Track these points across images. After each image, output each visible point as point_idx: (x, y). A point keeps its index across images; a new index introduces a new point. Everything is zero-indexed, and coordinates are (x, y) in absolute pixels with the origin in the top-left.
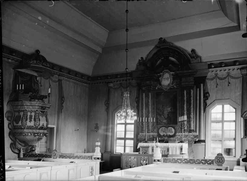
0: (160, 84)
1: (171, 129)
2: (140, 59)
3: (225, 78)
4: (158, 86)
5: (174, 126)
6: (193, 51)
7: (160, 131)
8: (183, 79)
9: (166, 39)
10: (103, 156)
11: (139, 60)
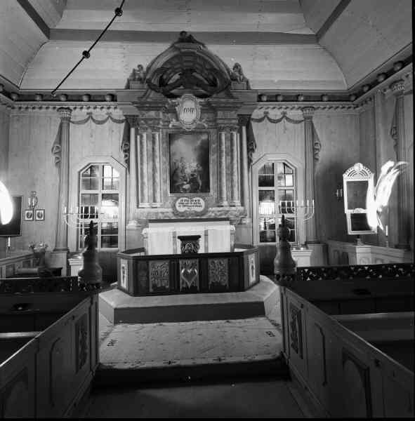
0: (177, 120)
1: (199, 201)
2: (137, 69)
3: (279, 121)
4: (174, 122)
5: (203, 194)
6: (237, 66)
7: (177, 204)
8: (220, 114)
9: (193, 35)
10: (100, 355)
11: (134, 70)
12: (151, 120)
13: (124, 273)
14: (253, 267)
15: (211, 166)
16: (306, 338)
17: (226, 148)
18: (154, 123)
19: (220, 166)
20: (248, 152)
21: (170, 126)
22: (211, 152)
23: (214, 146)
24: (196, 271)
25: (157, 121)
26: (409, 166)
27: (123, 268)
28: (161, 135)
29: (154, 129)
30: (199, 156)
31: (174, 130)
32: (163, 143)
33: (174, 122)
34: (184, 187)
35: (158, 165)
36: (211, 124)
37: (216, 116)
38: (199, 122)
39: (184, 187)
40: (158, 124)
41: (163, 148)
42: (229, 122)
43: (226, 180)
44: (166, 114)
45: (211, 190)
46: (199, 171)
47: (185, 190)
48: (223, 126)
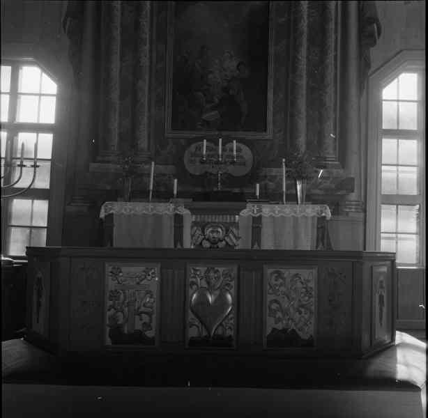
5: (250, 136)
13: (39, 296)
14: (381, 297)
16: (336, 68)
17: (309, 26)
20: (360, 46)
22: (272, 34)
24: (229, 297)
27: (39, 280)
34: (205, 117)
35: (145, 61)
39: (205, 117)
47: (207, 123)
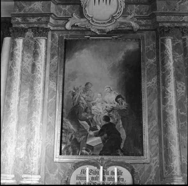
0: (82, 15)
12: (33, 16)
15: (145, 100)
18: (39, 22)
19: (165, 101)
21: (68, 26)
23: (152, 61)
25: (44, 19)
26: (102, 114)
28: (50, 41)
29: (41, 32)
30: (119, 84)
31: (73, 33)
32: (53, 56)
33: (75, 20)
36: (143, 22)
37: (154, 8)
38: (121, 20)
39: (89, 142)
40: (47, 22)
41: (52, 66)
42: (179, 19)
43: (179, 131)
44: (61, 6)
45: (147, 150)
46: (120, 111)
47: (90, 148)
48: (167, 25)
